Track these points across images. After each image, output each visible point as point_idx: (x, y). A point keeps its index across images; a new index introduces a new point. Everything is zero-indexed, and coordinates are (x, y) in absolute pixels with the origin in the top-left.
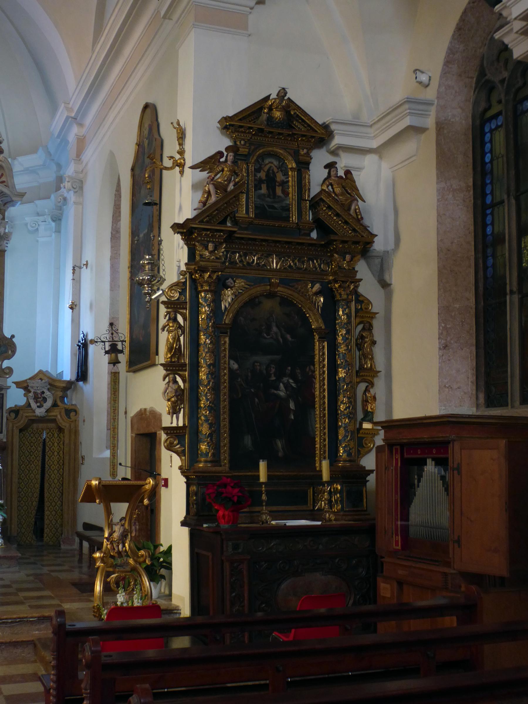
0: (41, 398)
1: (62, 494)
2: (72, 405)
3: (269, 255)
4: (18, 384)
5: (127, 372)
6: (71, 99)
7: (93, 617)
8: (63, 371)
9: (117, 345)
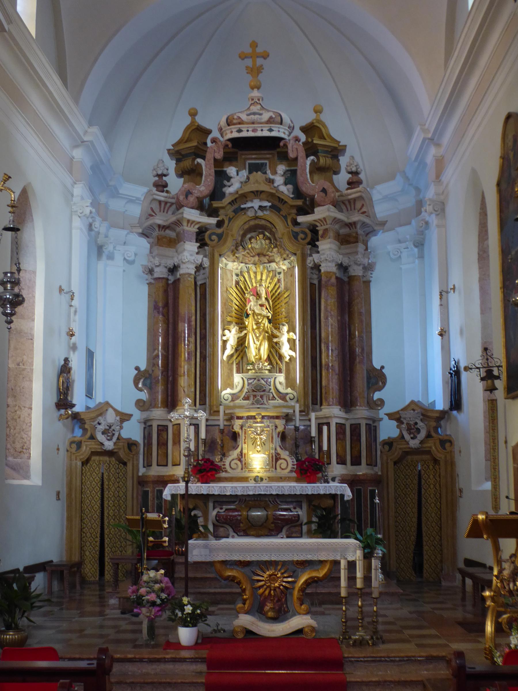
0: (413, 429)
1: (441, 528)
2: (447, 435)
4: (391, 416)
5: (505, 399)
6: (427, 120)
7: (484, 659)
8: (434, 401)
9: (493, 371)
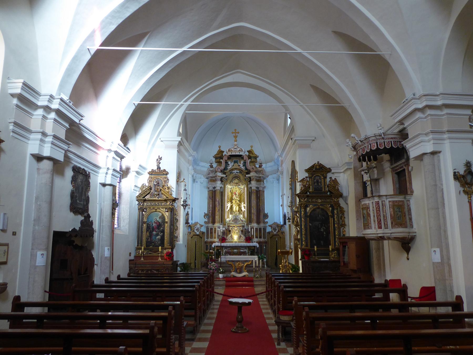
2: (283, 231)
3: (318, 199)
4: (269, 226)
